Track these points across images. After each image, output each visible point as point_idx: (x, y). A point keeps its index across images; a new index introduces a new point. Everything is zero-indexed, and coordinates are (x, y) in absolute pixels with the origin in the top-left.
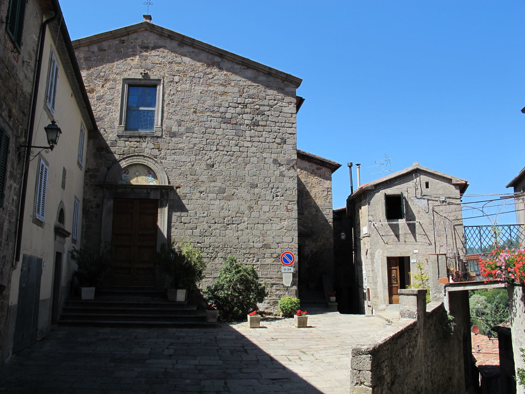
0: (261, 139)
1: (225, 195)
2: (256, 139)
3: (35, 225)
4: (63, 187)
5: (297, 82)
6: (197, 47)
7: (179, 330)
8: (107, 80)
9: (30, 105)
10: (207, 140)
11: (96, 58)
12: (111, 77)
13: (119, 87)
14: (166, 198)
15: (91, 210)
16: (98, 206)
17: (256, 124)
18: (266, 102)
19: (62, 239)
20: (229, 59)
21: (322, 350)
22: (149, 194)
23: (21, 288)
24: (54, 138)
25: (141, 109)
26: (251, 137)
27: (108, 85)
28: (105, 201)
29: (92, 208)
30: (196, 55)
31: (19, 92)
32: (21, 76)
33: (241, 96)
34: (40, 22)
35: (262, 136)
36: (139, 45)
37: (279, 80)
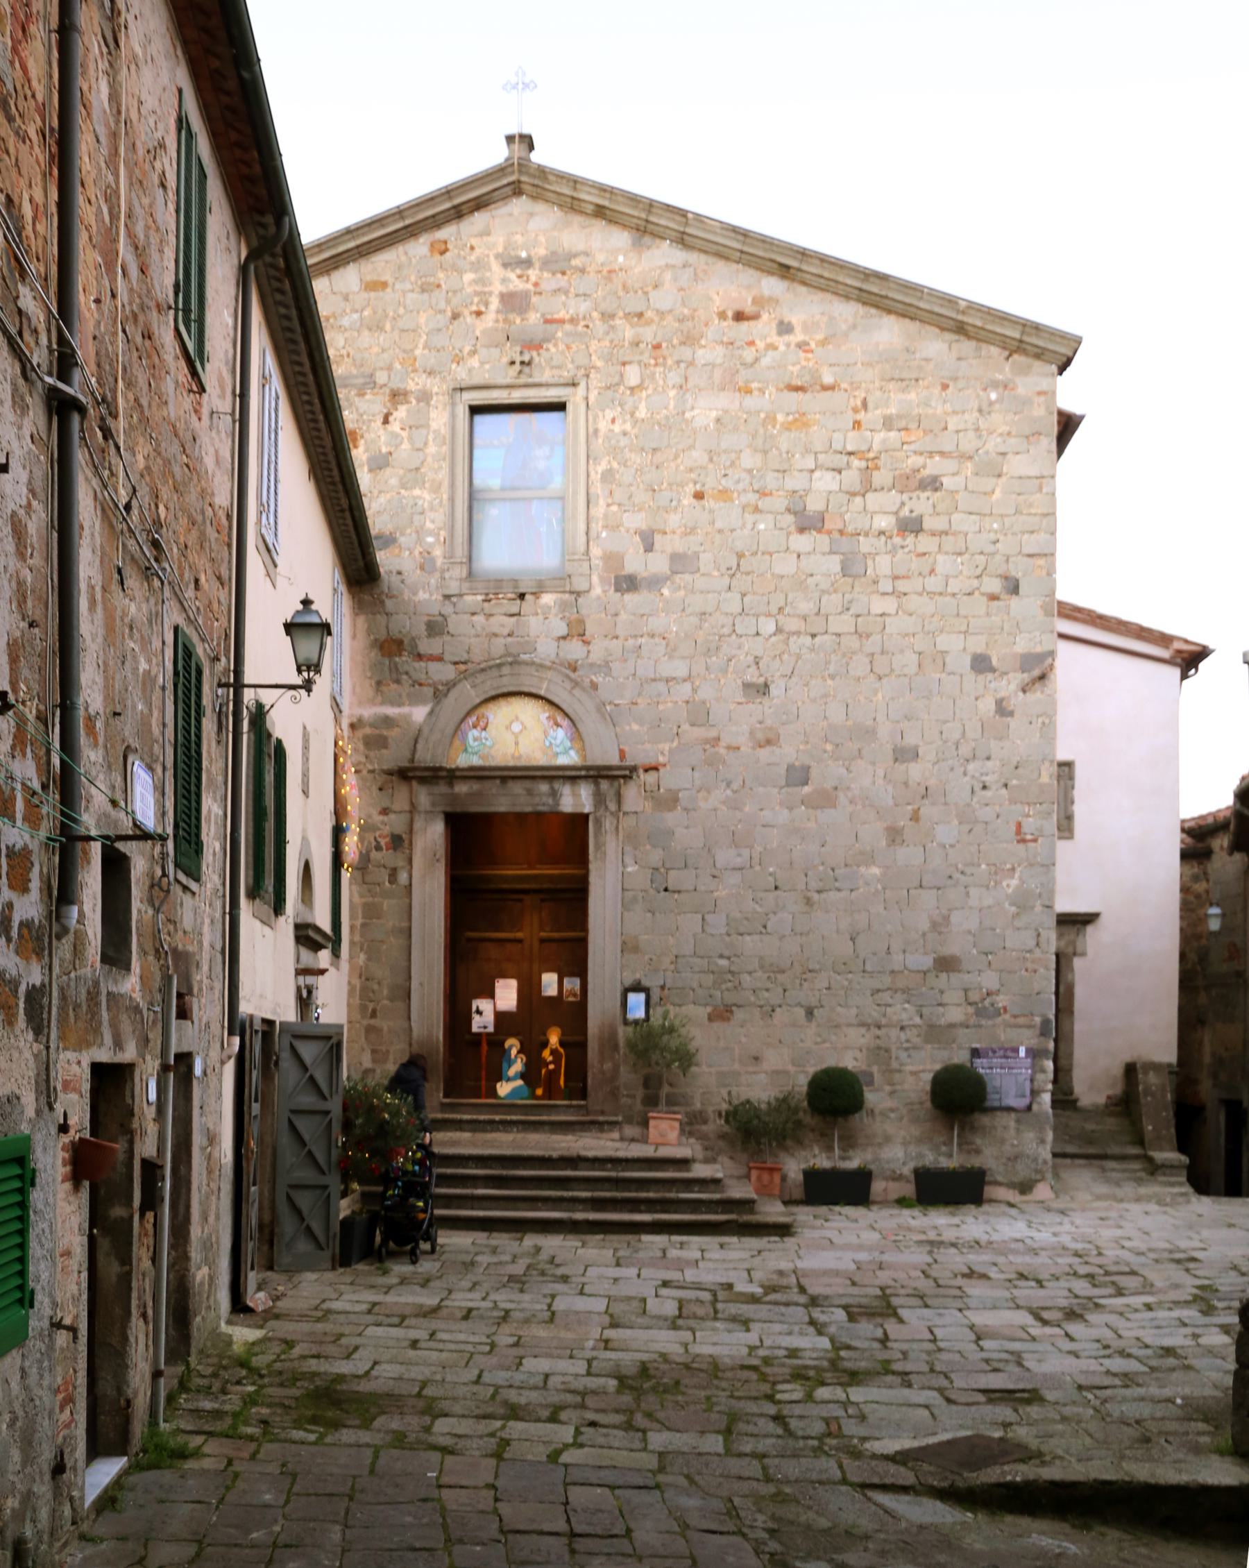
0: (933, 583)
1: (807, 789)
2: (917, 584)
5: (1059, 353)
6: (699, 243)
7: (676, 1238)
8: (397, 396)
9: (229, 546)
10: (743, 595)
11: (356, 316)
12: (411, 386)
14: (612, 806)
17: (911, 526)
19: (1140, 1071)
21: (1136, 1310)
22: (554, 794)
26: (896, 578)
27: (401, 413)
28: (418, 825)
30: (696, 278)
32: (209, 461)
34: (236, 262)
35: (932, 571)
36: (497, 256)
37: (994, 350)
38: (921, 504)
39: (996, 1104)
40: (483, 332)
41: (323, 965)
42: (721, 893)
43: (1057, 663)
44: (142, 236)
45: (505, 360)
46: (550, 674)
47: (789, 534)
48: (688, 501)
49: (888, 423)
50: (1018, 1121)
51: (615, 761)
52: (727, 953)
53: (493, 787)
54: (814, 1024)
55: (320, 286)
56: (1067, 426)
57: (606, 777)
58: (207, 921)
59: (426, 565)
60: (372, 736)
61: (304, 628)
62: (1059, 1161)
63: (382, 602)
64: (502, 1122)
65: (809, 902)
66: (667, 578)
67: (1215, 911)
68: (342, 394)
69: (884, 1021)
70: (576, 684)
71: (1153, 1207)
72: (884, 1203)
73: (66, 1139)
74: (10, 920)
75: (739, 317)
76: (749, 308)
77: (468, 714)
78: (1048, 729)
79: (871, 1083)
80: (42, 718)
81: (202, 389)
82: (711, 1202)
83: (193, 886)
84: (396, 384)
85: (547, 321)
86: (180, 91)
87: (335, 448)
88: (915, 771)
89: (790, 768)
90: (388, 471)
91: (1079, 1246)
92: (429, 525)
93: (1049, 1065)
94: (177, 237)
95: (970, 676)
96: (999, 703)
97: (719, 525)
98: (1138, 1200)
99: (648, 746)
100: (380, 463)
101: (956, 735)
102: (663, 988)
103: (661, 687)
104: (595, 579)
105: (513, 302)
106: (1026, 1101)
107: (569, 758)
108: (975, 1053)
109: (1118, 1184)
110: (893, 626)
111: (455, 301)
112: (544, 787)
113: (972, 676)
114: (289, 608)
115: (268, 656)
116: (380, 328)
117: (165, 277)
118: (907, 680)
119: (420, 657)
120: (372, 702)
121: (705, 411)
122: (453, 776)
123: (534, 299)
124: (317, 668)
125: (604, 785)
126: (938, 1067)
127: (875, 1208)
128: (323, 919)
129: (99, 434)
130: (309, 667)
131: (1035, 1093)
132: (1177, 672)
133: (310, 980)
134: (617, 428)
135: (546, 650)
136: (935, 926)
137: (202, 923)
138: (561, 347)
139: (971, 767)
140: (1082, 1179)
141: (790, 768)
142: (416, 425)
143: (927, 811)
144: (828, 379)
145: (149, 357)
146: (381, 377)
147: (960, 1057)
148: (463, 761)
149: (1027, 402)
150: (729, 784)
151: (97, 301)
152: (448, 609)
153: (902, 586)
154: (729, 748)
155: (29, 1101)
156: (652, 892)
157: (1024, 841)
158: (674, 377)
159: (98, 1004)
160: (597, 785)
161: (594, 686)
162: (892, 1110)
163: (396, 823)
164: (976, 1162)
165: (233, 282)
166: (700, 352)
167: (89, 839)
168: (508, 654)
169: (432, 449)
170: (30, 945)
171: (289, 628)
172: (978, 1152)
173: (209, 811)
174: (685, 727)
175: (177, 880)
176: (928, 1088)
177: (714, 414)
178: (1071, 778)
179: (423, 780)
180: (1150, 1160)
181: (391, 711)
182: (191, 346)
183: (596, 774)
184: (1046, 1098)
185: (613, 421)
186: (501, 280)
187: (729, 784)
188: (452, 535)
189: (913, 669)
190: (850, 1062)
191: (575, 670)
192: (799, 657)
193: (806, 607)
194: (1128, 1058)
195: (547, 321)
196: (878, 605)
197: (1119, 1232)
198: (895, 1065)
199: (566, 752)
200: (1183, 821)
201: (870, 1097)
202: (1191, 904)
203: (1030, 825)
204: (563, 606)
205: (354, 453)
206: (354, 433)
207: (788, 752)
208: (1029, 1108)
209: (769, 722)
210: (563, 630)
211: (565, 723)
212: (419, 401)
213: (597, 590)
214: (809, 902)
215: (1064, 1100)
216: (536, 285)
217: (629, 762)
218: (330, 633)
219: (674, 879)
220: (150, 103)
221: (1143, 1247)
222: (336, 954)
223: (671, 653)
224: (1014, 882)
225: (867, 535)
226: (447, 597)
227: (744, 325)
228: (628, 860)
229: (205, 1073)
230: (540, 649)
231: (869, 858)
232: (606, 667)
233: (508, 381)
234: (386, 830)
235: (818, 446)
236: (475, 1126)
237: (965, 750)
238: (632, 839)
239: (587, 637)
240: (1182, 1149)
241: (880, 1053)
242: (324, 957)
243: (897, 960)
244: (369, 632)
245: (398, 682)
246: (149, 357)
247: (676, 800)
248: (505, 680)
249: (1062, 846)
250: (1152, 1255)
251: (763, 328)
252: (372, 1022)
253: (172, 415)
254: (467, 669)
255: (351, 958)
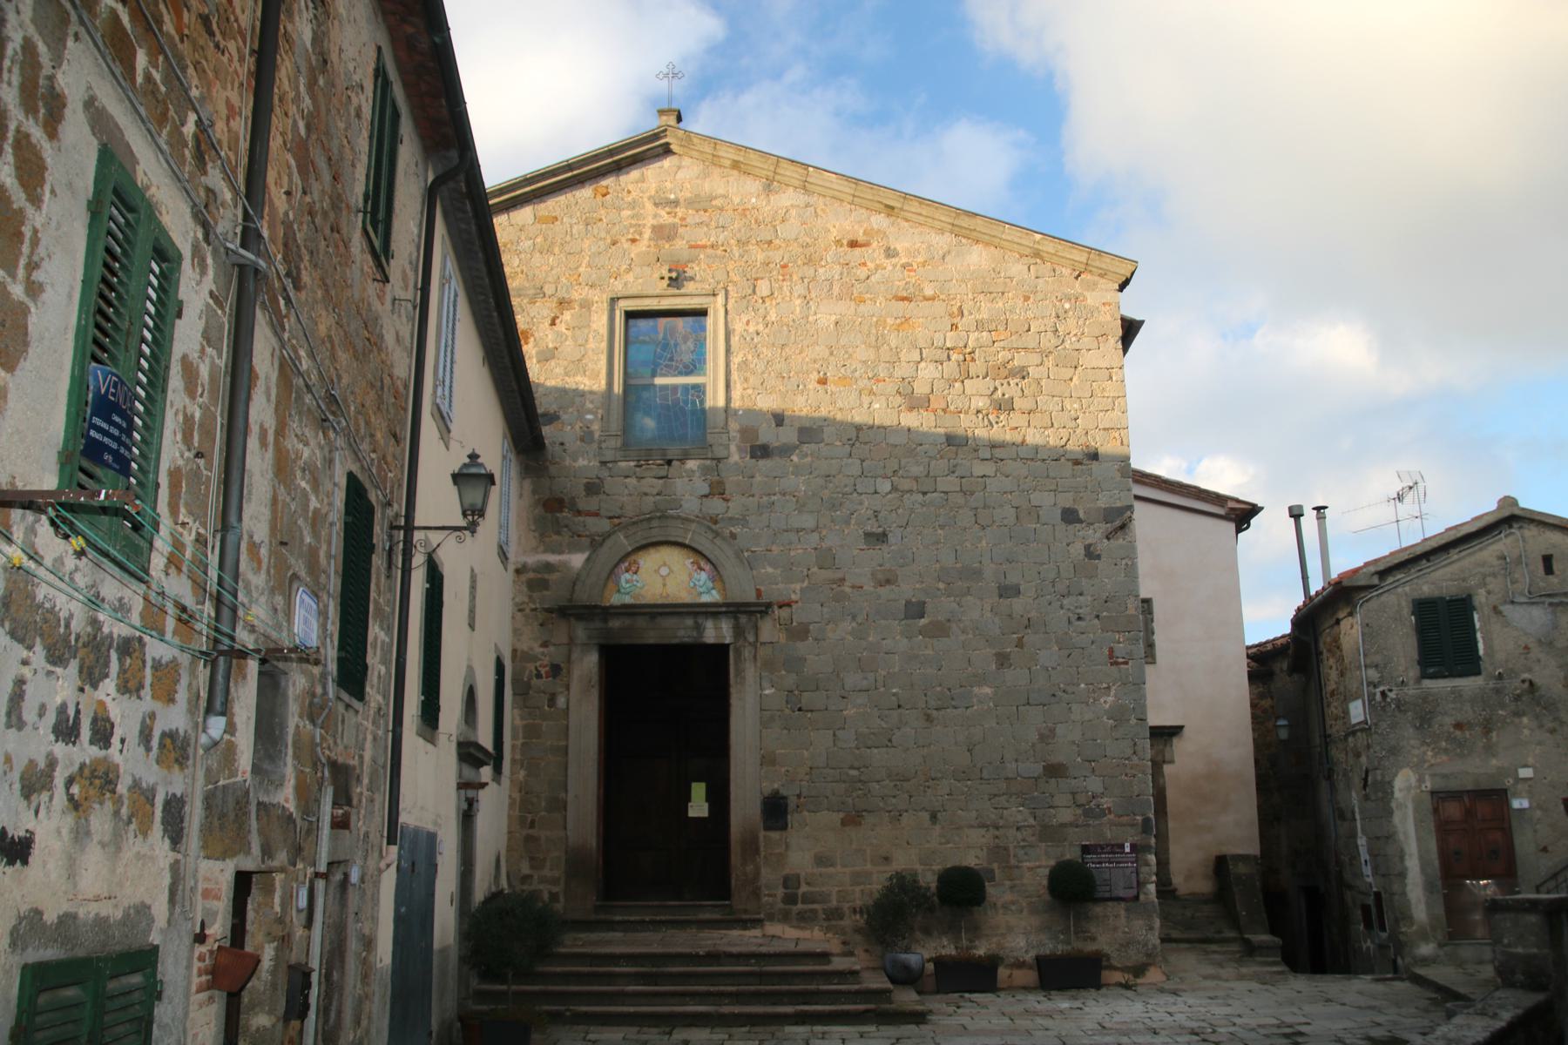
1: (923, 621)
3: (421, 741)
4: (472, 626)
7: (819, 1028)
8: (563, 304)
12: (575, 295)
13: (600, 322)
14: (751, 639)
15: (535, 681)
16: (556, 670)
18: (1030, 340)
20: (914, 217)
22: (699, 628)
23: (399, 920)
24: (479, 502)
25: (659, 381)
27: (567, 316)
28: (575, 656)
29: (539, 676)
31: (387, 381)
32: (389, 339)
33: (954, 327)
38: (1010, 390)
39: (1107, 895)
40: (638, 255)
41: (484, 780)
42: (850, 712)
43: (1135, 516)
44: (335, 151)
45: (657, 276)
46: (693, 526)
47: (899, 412)
48: (812, 385)
49: (979, 326)
50: (1127, 910)
51: (752, 598)
52: (856, 764)
53: (641, 622)
54: (938, 827)
55: (500, 222)
56: (1130, 329)
57: (745, 612)
58: (369, 737)
59: (587, 437)
60: (534, 580)
61: (470, 477)
62: (1167, 945)
63: (547, 468)
64: (652, 922)
65: (929, 718)
66: (796, 447)
67: (1281, 722)
68: (515, 301)
69: (1001, 823)
70: (717, 534)
71: (1254, 985)
72: (1011, 989)
73: (203, 949)
74: (151, 730)
75: (853, 244)
76: (861, 238)
77: (622, 560)
78: (1131, 571)
79: (992, 879)
80: (200, 541)
81: (386, 280)
82: (849, 992)
83: (356, 704)
84: (562, 294)
85: (691, 247)
86: (379, 49)
87: (506, 334)
88: (1018, 605)
89: (908, 603)
90: (553, 363)
91: (1194, 1025)
92: (589, 406)
93: (1152, 858)
94: (370, 157)
95: (1062, 526)
96: (1088, 548)
97: (840, 404)
98: (1241, 978)
99: (781, 586)
100: (547, 356)
101: (1052, 575)
102: (799, 796)
103: (793, 537)
104: (733, 448)
105: (664, 233)
106: (1134, 892)
107: (714, 596)
108: (1086, 849)
109: (1221, 965)
110: (993, 485)
111: (614, 231)
112: (689, 622)
113: (1064, 526)
114: (458, 460)
115: (437, 501)
116: (550, 251)
117: (358, 186)
118: (1006, 530)
119: (579, 513)
120: (535, 550)
121: (826, 315)
122: (608, 612)
123: (681, 230)
124: (481, 513)
125: (743, 619)
126: (1052, 863)
127: (1002, 994)
128: (485, 738)
129: (282, 302)
130: (474, 513)
131: (1140, 884)
132: (1232, 526)
133: (471, 793)
134: (752, 329)
135: (690, 506)
136: (1042, 737)
137: (365, 739)
138: (703, 266)
139: (1065, 602)
140: (1188, 962)
141: (908, 603)
142: (582, 325)
143: (1031, 638)
144: (929, 292)
145: (337, 247)
146: (549, 290)
147: (1072, 854)
148: (616, 599)
149: (1092, 311)
150: (854, 618)
151: (288, 193)
152: (604, 473)
153: (998, 453)
154: (853, 587)
155: (160, 910)
156: (787, 711)
157: (1117, 663)
158: (800, 289)
159: (247, 814)
160: (736, 619)
161: (733, 536)
162: (1013, 903)
163: (553, 654)
164: (1090, 947)
165: (420, 200)
166: (821, 271)
167: (243, 655)
168: (658, 510)
169: (592, 345)
170: (173, 755)
171: (457, 478)
172: (1093, 939)
173: (376, 638)
174: (815, 569)
175: (339, 698)
176: (1045, 882)
177: (833, 318)
178: (1151, 613)
179: (579, 617)
180: (1247, 942)
181: (553, 558)
182: (377, 244)
183: (733, 610)
184: (1152, 888)
185: (748, 323)
186: (653, 216)
187: (854, 618)
188: (608, 411)
189: (1012, 520)
190: (971, 860)
191: (716, 522)
192: (912, 511)
193: (916, 470)
194: (1215, 851)
195: (691, 247)
196: (979, 469)
197: (1228, 1010)
198: (1013, 862)
199: (708, 592)
200: (1248, 648)
201: (990, 890)
202: (1260, 717)
203: (1121, 649)
204: (705, 471)
205: (525, 348)
206: (525, 332)
207: (907, 590)
208: (1137, 898)
209: (887, 566)
210: (706, 490)
211: (708, 567)
212: (582, 306)
213: (735, 457)
214: (929, 718)
215: (1166, 891)
216: (683, 219)
217: (765, 600)
218: (493, 483)
219: (806, 699)
220: (350, 52)
221: (1253, 1023)
222: (498, 770)
223: (801, 507)
224: (1110, 699)
225: (967, 413)
226: (603, 463)
227: (857, 251)
228: (765, 684)
229: (362, 880)
230: (686, 506)
231: (981, 680)
232: (743, 521)
233: (658, 292)
234: (546, 661)
235: (921, 344)
236: (627, 926)
237: (1061, 587)
238: (769, 665)
239: (727, 496)
240: (1273, 932)
241: (998, 852)
242: (486, 772)
243: (1011, 767)
244: (534, 492)
245: (558, 533)
246: (337, 247)
247: (807, 632)
248: (654, 532)
249: (1149, 669)
250: (1263, 1031)
251: (874, 253)
252: (531, 831)
253: (357, 296)
254: (620, 522)
255: (512, 773)
